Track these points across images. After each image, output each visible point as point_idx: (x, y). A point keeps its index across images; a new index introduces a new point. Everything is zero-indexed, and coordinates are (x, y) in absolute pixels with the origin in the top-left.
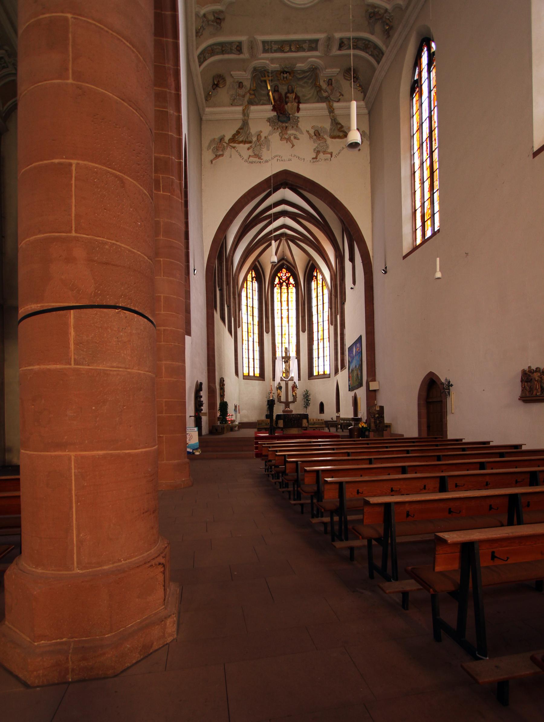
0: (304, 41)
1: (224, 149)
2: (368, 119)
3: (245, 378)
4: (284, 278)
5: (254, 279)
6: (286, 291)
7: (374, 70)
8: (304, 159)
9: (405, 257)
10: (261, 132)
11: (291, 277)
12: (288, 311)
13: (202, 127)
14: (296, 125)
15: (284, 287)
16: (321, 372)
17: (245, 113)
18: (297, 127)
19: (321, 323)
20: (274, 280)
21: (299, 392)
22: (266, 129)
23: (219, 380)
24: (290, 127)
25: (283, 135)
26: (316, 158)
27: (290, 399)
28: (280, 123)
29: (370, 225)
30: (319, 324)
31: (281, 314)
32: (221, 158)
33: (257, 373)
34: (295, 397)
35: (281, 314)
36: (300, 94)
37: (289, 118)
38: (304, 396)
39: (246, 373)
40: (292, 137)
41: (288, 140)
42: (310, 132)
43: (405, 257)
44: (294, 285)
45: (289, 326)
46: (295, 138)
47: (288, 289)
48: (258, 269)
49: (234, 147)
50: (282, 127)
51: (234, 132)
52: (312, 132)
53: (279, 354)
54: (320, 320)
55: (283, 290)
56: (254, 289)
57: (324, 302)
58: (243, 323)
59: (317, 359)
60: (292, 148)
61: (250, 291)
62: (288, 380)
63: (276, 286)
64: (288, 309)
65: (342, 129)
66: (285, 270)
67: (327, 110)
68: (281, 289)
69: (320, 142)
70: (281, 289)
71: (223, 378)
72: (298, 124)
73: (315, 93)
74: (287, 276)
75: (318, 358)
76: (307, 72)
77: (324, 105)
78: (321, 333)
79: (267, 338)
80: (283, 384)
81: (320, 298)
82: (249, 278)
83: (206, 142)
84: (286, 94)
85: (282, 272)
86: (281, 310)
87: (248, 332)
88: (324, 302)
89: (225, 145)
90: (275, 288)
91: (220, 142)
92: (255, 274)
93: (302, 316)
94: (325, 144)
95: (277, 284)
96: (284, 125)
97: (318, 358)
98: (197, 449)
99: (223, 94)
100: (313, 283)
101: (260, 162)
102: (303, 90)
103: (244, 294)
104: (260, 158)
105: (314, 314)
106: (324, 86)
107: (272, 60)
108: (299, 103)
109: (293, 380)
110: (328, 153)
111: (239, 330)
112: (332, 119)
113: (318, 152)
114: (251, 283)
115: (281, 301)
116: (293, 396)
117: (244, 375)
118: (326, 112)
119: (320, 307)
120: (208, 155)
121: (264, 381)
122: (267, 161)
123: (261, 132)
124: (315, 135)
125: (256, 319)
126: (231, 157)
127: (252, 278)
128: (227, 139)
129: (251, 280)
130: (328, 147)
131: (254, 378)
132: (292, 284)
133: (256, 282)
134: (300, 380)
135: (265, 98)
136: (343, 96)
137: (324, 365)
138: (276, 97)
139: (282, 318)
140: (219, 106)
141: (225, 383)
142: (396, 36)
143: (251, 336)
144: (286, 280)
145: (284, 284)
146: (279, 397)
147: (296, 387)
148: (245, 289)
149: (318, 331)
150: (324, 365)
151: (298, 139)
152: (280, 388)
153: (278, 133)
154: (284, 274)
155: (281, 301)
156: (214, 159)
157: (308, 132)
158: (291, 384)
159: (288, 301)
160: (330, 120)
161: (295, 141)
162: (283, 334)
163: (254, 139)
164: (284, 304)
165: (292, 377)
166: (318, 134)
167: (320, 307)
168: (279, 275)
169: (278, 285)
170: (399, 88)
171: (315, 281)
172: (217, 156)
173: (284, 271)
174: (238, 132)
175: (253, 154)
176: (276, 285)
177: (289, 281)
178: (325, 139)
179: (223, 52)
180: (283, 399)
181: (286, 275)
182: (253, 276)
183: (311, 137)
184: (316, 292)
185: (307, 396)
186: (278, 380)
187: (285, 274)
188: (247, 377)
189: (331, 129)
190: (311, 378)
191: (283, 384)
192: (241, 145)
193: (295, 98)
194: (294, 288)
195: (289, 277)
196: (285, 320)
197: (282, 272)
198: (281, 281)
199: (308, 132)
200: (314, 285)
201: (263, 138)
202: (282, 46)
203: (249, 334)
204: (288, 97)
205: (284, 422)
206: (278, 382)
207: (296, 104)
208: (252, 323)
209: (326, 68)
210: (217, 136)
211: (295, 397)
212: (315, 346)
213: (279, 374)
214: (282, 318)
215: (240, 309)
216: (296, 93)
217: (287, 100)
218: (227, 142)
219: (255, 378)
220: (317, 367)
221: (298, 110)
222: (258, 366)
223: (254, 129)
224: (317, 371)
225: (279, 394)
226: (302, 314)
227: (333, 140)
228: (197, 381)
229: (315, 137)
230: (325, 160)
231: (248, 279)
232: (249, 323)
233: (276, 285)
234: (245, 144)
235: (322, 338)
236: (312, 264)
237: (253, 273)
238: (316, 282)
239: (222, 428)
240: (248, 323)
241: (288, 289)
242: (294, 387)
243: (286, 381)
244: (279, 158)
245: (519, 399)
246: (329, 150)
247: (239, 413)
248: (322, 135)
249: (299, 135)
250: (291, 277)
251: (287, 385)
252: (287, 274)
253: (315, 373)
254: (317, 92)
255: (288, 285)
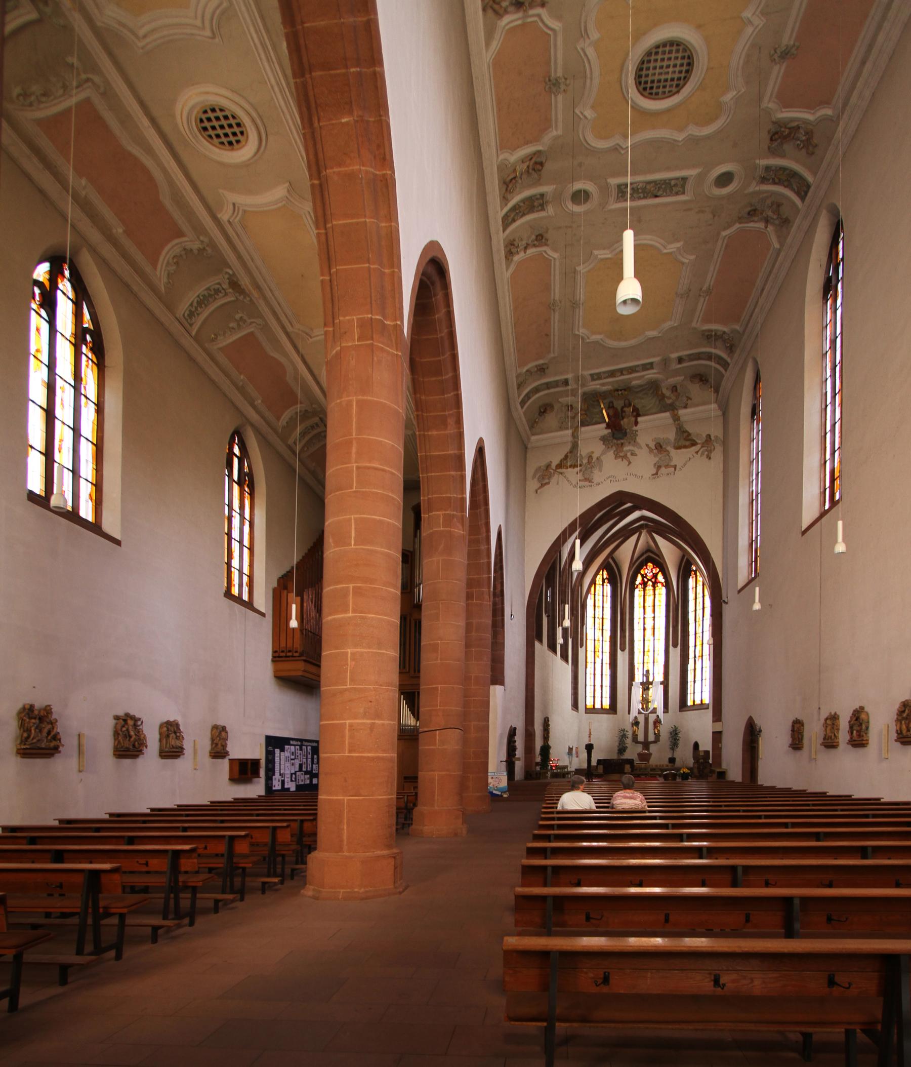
0: (638, 366)
1: (549, 478)
2: (722, 421)
3: (588, 711)
4: (650, 575)
5: (606, 581)
6: (651, 592)
7: (723, 376)
8: (642, 477)
9: (739, 591)
10: (593, 452)
11: (660, 573)
12: (654, 620)
13: (527, 456)
14: (633, 441)
15: (649, 588)
16: (698, 702)
17: (575, 436)
18: (635, 442)
19: (699, 635)
20: (634, 578)
21: (664, 730)
22: (597, 448)
23: (543, 719)
24: (627, 444)
25: (618, 453)
26: (657, 474)
27: (651, 738)
28: (615, 441)
29: (720, 544)
30: (697, 635)
31: (644, 624)
32: (546, 487)
33: (606, 704)
34: (657, 736)
35: (644, 624)
36: (639, 406)
37: (625, 434)
38: (671, 734)
39: (590, 704)
40: (629, 454)
41: (625, 457)
42: (650, 446)
43: (739, 591)
44: (664, 584)
45: (654, 640)
46: (632, 454)
47: (654, 590)
48: (612, 567)
49: (561, 473)
50: (617, 444)
51: (563, 456)
52: (652, 445)
53: (639, 678)
54: (699, 630)
55: (647, 592)
56: (605, 594)
57: (705, 606)
58: (588, 641)
59: (693, 683)
60: (628, 465)
61: (599, 598)
62: (648, 712)
63: (637, 588)
64: (654, 617)
65: (690, 437)
66: (651, 565)
67: (671, 419)
68: (644, 590)
69: (660, 456)
70: (644, 590)
71: (548, 718)
72: (636, 439)
73: (658, 402)
74: (654, 572)
75: (695, 682)
76: (646, 385)
77: (667, 414)
78: (699, 648)
79: (622, 657)
80: (641, 719)
81: (700, 600)
82: (599, 580)
83: (530, 471)
84: (622, 408)
85: (647, 568)
86: (644, 618)
87: (594, 652)
88: (694, 612)
89: (552, 471)
90: (637, 590)
91: (547, 469)
92: (608, 574)
93: (673, 626)
94: (668, 457)
95: (640, 584)
96: (619, 442)
97: (695, 682)
98: (505, 792)
99: (551, 419)
100: (691, 580)
101: (591, 486)
102: (643, 401)
103: (590, 602)
104: (590, 481)
105: (690, 634)
106: (667, 393)
107: (603, 385)
108: (638, 415)
109: (656, 713)
110: (672, 466)
111: (581, 652)
112: (677, 428)
113: (659, 467)
114: (601, 586)
115: (644, 607)
116: (655, 734)
117: (587, 707)
118: (671, 421)
119: (699, 612)
120: (532, 485)
121: (616, 714)
122: (598, 484)
123: (593, 452)
124: (656, 448)
125: (607, 634)
126: (558, 484)
127: (603, 581)
128: (554, 466)
129: (601, 583)
130: (670, 459)
131: (602, 711)
132: (660, 582)
133: (608, 585)
134: (667, 712)
135: (598, 416)
136: (691, 399)
137: (702, 692)
138: (611, 413)
139: (644, 629)
140: (546, 433)
141: (550, 723)
142: (738, 351)
143: (598, 657)
144: (652, 579)
145: (650, 583)
146: (635, 736)
147: (660, 722)
148: (593, 596)
149: (695, 646)
150: (702, 692)
151: (636, 455)
152: (636, 723)
153: (613, 451)
154: (649, 570)
155: (644, 607)
156: (540, 488)
157: (647, 445)
158: (652, 718)
159: (654, 606)
160: (675, 429)
161: (631, 458)
162: (646, 650)
163: (585, 461)
164: (649, 610)
165: (655, 709)
166: (659, 447)
167: (699, 612)
168: (642, 572)
169: (640, 586)
170: (740, 408)
171: (693, 577)
172: (542, 485)
173: (650, 565)
174: (566, 457)
175: (583, 478)
176: (637, 585)
177: (656, 578)
178: (668, 451)
179: (548, 388)
180: (641, 738)
181: (652, 572)
182: (605, 576)
183: (651, 450)
184: (694, 592)
185: (675, 734)
186: (634, 713)
187: (652, 569)
188: (592, 711)
189: (675, 439)
190: (684, 709)
191: (641, 719)
192: (570, 470)
193: (633, 411)
194: (664, 588)
195: (657, 574)
196: (649, 632)
197: (647, 568)
198: (646, 580)
199: (647, 445)
200: (691, 582)
201: (594, 459)
202: (612, 374)
203: (597, 653)
204: (625, 412)
205: (604, 768)
206: (634, 715)
207: (633, 419)
208: (601, 639)
209: (667, 379)
210: (543, 463)
211: (657, 736)
212: (691, 666)
213: (636, 705)
214: (644, 629)
215: (583, 623)
216: (634, 406)
217: (624, 414)
218: (554, 468)
219: (603, 711)
220: (692, 695)
221: (636, 423)
222: (608, 695)
223: (584, 450)
224: (692, 699)
225: (635, 732)
226: (673, 623)
227: (678, 451)
228: (511, 726)
229: (655, 451)
230: (668, 474)
231: (597, 582)
232: (596, 639)
233: (637, 585)
234: (574, 468)
235: (701, 655)
236: (687, 559)
237: (605, 573)
238: (694, 578)
239: (537, 774)
240: (595, 640)
241: (654, 590)
242: (657, 722)
243: (645, 714)
244: (612, 479)
245: (848, 744)
246: (672, 464)
247: (577, 757)
248: (664, 447)
249: (636, 450)
250: (660, 573)
251: (647, 719)
252: (654, 570)
253: (690, 703)
254: (660, 401)
255: (654, 586)
